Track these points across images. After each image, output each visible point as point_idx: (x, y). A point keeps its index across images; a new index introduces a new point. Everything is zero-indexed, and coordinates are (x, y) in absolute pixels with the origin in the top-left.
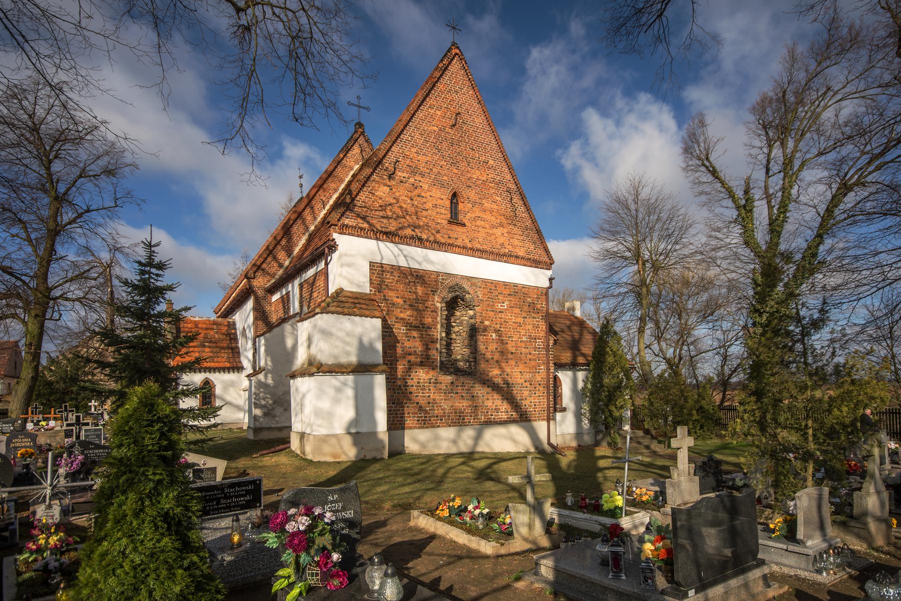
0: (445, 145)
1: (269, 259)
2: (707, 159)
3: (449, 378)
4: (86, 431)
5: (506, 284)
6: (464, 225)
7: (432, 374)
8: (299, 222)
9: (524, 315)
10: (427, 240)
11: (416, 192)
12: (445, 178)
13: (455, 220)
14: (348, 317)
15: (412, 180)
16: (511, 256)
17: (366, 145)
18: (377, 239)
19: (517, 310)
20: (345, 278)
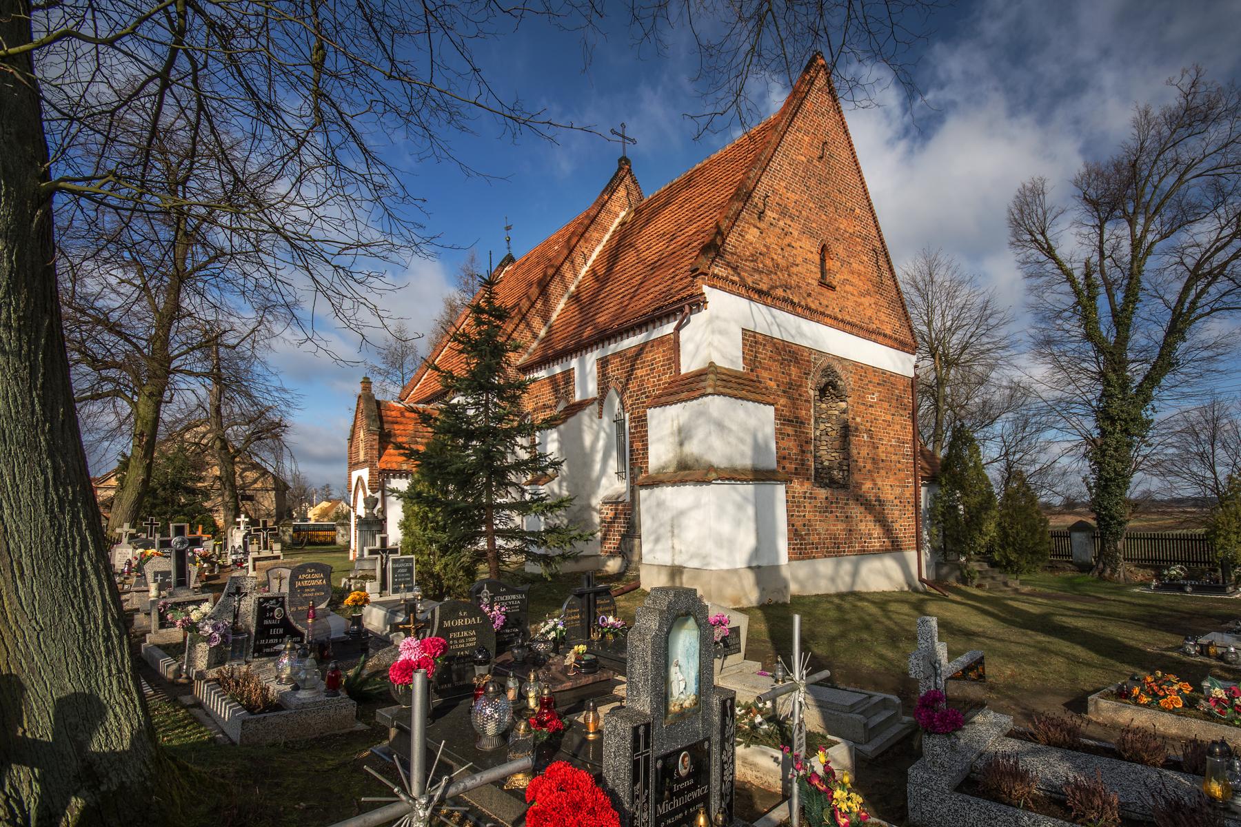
0: (813, 182)
1: (522, 326)
2: (1043, 233)
3: (822, 493)
4: (395, 561)
5: (875, 370)
6: (833, 288)
7: (807, 486)
8: (557, 279)
9: (893, 411)
10: (800, 306)
11: (787, 240)
12: (814, 225)
13: (825, 284)
14: (740, 401)
15: (781, 223)
16: (879, 334)
17: (632, 186)
18: (750, 299)
19: (886, 405)
20: (716, 348)
